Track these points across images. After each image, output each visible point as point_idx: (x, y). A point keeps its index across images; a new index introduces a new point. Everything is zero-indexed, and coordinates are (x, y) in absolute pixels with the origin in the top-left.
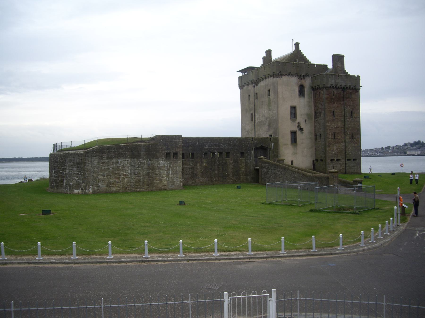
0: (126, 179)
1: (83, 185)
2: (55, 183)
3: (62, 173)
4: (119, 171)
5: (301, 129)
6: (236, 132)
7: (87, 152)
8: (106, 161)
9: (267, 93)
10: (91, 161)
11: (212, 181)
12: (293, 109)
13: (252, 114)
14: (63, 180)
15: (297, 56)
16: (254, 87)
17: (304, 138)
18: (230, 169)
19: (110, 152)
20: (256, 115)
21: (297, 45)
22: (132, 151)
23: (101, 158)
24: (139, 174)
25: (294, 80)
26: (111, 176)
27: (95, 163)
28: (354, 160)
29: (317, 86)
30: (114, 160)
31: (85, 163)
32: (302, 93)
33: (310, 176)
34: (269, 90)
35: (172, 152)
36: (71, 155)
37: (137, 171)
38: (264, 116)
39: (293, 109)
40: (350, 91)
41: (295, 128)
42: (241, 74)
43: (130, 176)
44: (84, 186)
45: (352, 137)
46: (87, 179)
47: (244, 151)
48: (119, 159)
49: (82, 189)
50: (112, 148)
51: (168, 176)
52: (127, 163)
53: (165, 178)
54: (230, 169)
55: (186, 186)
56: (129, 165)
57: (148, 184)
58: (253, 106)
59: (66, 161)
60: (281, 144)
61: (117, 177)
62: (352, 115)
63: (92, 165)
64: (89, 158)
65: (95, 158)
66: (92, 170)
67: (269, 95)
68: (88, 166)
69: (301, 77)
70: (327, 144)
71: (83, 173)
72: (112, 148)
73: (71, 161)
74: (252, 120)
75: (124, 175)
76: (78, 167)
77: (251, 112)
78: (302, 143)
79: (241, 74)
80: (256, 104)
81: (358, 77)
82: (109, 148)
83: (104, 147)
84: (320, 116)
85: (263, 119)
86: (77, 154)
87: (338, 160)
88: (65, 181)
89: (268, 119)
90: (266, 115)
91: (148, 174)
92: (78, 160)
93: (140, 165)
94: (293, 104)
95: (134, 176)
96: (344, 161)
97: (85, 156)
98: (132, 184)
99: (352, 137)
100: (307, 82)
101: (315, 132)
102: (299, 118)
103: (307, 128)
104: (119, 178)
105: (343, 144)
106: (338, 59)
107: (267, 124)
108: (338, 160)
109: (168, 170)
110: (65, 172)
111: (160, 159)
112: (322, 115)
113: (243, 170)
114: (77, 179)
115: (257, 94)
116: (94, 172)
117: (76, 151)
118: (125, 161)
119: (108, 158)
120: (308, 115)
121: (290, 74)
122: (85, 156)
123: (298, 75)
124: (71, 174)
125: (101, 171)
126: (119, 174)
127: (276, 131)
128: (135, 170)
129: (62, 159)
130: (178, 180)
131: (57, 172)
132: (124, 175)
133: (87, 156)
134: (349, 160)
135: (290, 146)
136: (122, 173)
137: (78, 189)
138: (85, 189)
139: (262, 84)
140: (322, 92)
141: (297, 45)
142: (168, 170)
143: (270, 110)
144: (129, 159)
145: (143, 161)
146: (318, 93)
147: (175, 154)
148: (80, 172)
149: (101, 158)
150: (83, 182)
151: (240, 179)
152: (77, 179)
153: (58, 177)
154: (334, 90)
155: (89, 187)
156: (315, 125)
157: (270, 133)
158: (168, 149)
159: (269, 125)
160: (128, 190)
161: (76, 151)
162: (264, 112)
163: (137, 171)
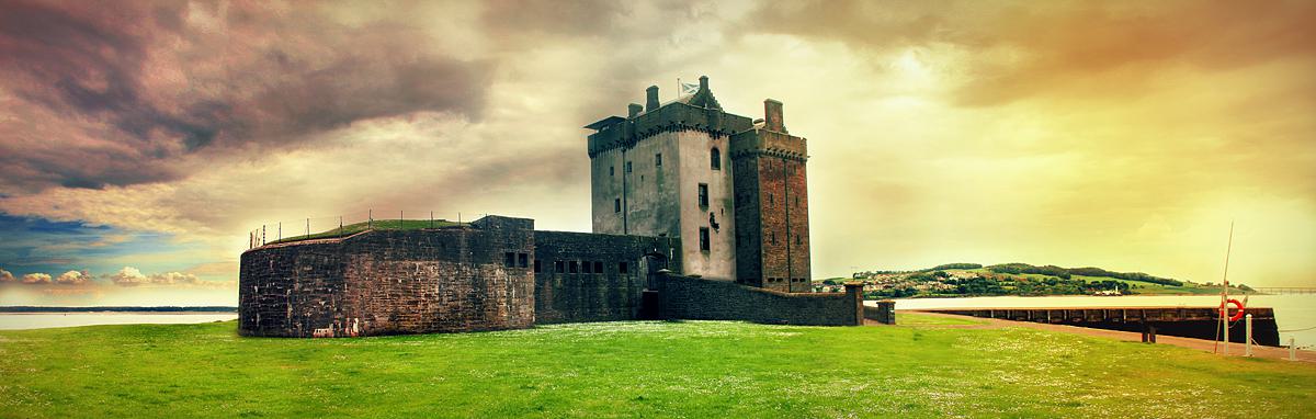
0: (430, 306)
1: (339, 316)
2: (261, 316)
3: (280, 291)
4: (417, 286)
5: (716, 226)
6: (591, 231)
7: (349, 242)
8: (391, 263)
9: (654, 160)
10: (358, 263)
11: (571, 317)
12: (704, 187)
13: (618, 201)
14: (286, 307)
15: (704, 99)
16: (624, 151)
17: (720, 242)
18: (602, 294)
19: (398, 243)
20: (628, 200)
21: (704, 80)
22: (443, 245)
23: (379, 257)
24: (456, 295)
25: (704, 137)
26: (399, 296)
27: (367, 267)
28: (802, 280)
29: (743, 151)
30: (407, 263)
31: (343, 266)
32: (715, 164)
33: (792, 298)
34: (659, 156)
35: (517, 251)
36: (308, 247)
37: (451, 288)
38: (648, 201)
39: (704, 187)
40: (795, 163)
41: (707, 224)
42: (593, 132)
43: (437, 299)
44: (340, 319)
45: (798, 242)
46: (348, 303)
47: (626, 260)
48: (416, 260)
49: (335, 326)
50: (403, 235)
51: (509, 302)
52: (433, 270)
53: (505, 305)
54: (602, 294)
55: (541, 320)
56: (436, 274)
57: (474, 315)
58: (622, 186)
59: (293, 262)
60: (684, 250)
61: (413, 299)
62: (797, 205)
63: (359, 270)
64: (354, 256)
65: (367, 255)
66: (360, 283)
67: (659, 163)
68: (352, 274)
69: (715, 134)
70: (763, 252)
71: (340, 289)
72: (403, 235)
73: (306, 262)
74: (618, 209)
75: (426, 296)
76: (327, 276)
77: (617, 197)
78: (718, 250)
79: (593, 132)
80: (628, 180)
81: (712, 169)
82: (397, 234)
83: (387, 231)
84: (749, 202)
85: (646, 207)
86: (325, 245)
87: (779, 280)
88: (290, 309)
89: (657, 207)
90: (652, 201)
91: (473, 296)
92: (326, 259)
93: (458, 275)
94: (704, 181)
95: (445, 299)
96: (787, 281)
97: (344, 250)
98: (443, 317)
99: (798, 242)
100: (723, 144)
101: (737, 231)
102: (713, 207)
103: (725, 223)
104: (416, 303)
105: (785, 252)
106: (773, 108)
107: (654, 215)
108: (779, 280)
109: (510, 287)
110: (292, 287)
111: (495, 265)
112: (752, 202)
113: (624, 295)
114: (323, 303)
115: (630, 163)
116: (364, 286)
117: (321, 241)
118: (429, 265)
119: (395, 257)
120: (725, 200)
121: (697, 128)
122: (344, 250)
123: (709, 132)
124: (308, 292)
125: (379, 286)
126: (416, 294)
127: (676, 226)
128: (448, 285)
129: (282, 259)
130: (527, 310)
131: (269, 290)
132: (426, 296)
133: (351, 251)
134: (794, 280)
135: (699, 255)
136: (423, 292)
137: (326, 326)
138: (344, 326)
139: (642, 145)
140: (753, 161)
141: (704, 80)
142: (510, 287)
143: (660, 190)
144: (437, 262)
145: (464, 268)
146: (744, 163)
147: (523, 257)
148: (329, 286)
149: (379, 257)
150: (339, 310)
151: (619, 312)
152: (323, 303)
153: (272, 302)
154: (771, 159)
155: (353, 322)
156: (736, 220)
157: (661, 231)
158: (510, 246)
159: (660, 217)
160: (435, 327)
161: (321, 241)
162: (646, 195)
163: (451, 288)
